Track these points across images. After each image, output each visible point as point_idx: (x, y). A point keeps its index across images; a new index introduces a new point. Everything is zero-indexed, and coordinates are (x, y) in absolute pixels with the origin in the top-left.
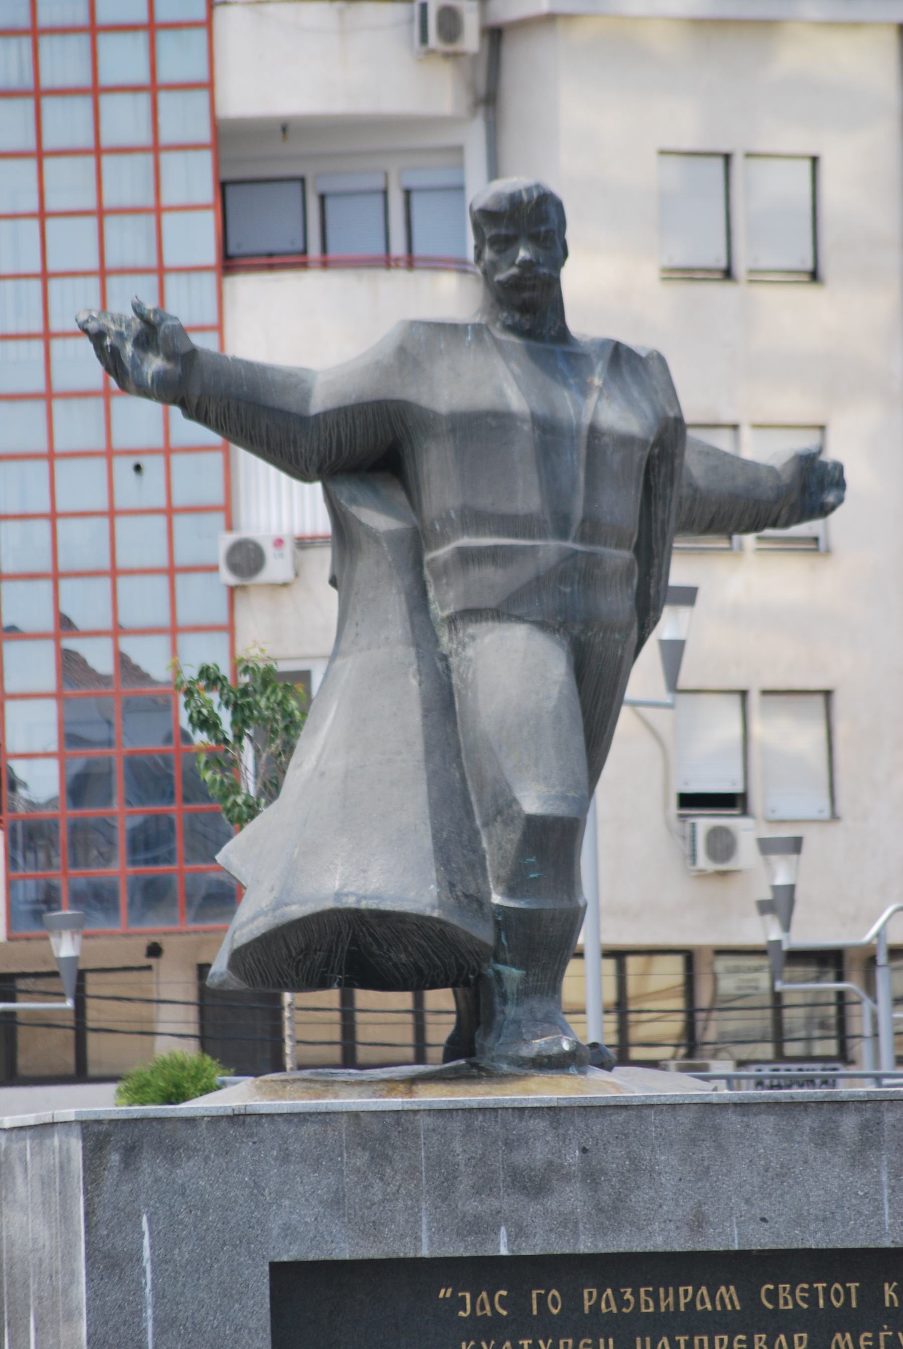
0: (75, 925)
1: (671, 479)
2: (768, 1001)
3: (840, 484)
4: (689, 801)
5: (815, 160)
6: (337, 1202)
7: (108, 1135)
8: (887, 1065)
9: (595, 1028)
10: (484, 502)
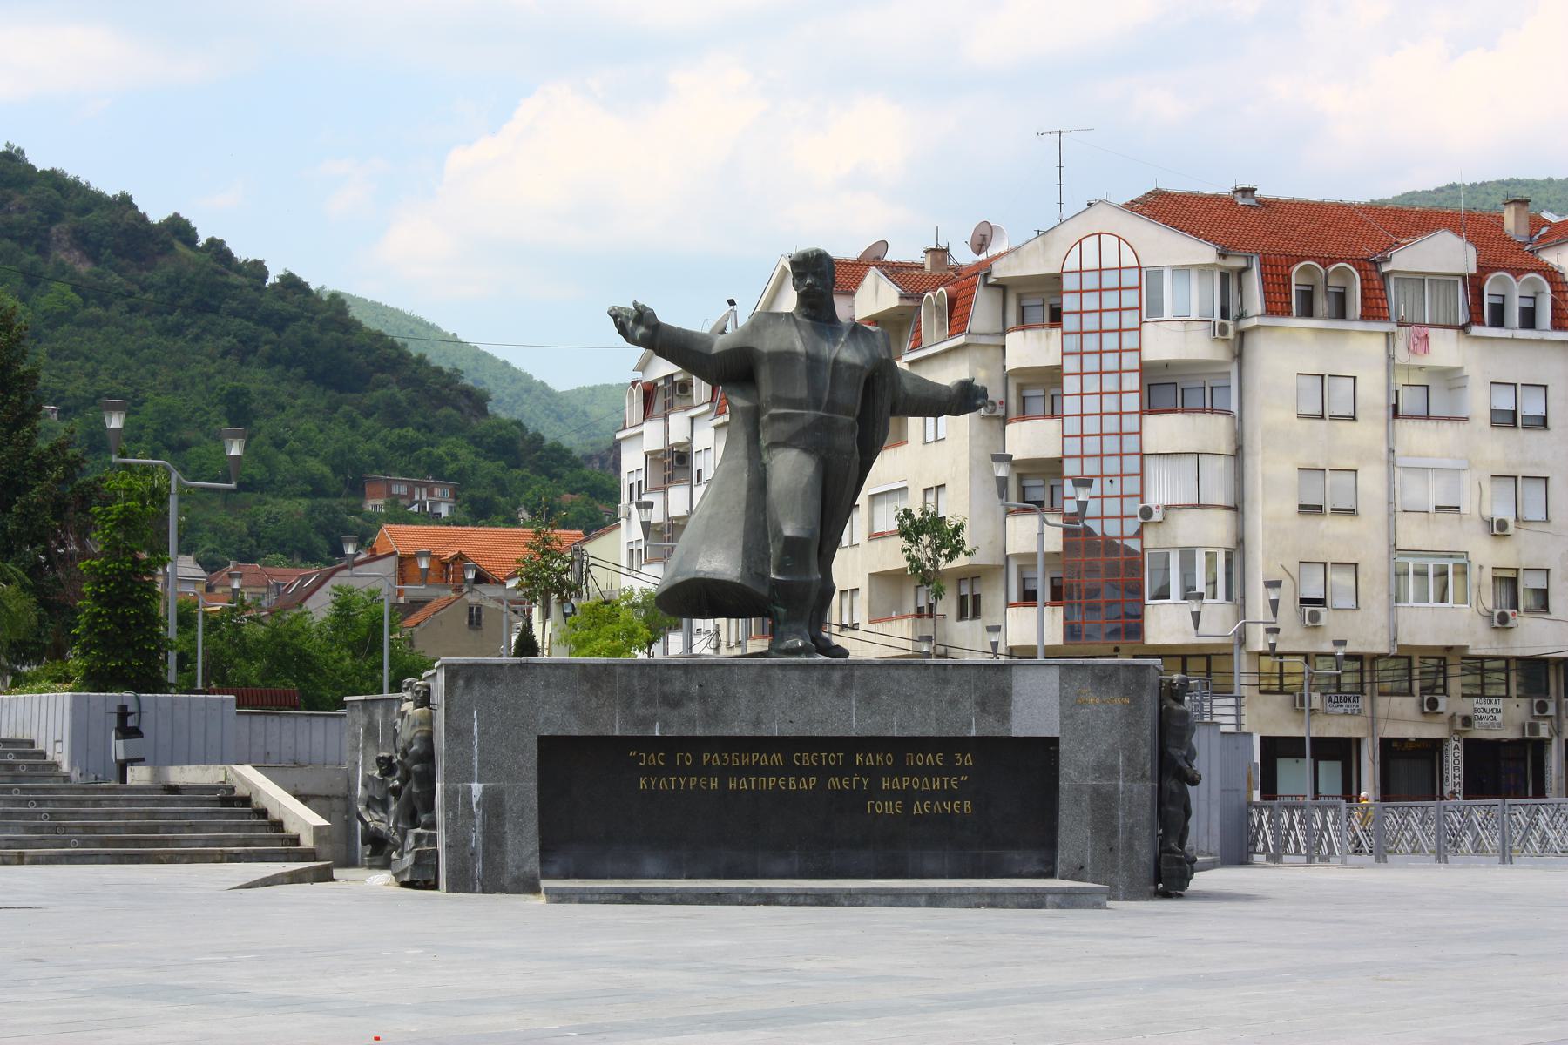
4: (1304, 601)
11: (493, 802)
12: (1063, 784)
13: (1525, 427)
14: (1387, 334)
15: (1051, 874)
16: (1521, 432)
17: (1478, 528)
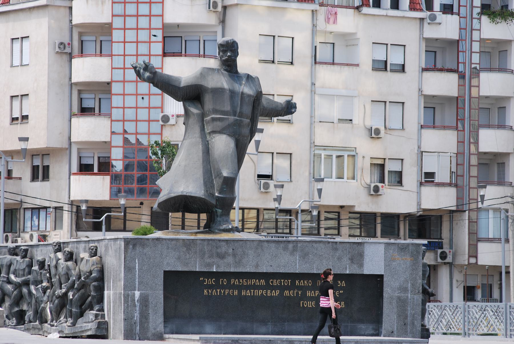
0: (124, 197)
1: (259, 104)
2: (275, 220)
3: (296, 108)
4: (260, 176)
5: (293, 38)
6: (179, 258)
7: (130, 241)
8: (299, 235)
9: (237, 224)
10: (218, 108)
11: (144, 301)
12: (385, 295)
13: (392, 71)
14: (313, 11)
15: (378, 335)
16: (389, 74)
17: (364, 133)
